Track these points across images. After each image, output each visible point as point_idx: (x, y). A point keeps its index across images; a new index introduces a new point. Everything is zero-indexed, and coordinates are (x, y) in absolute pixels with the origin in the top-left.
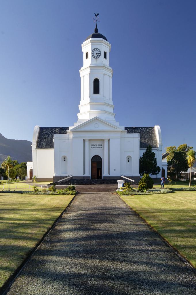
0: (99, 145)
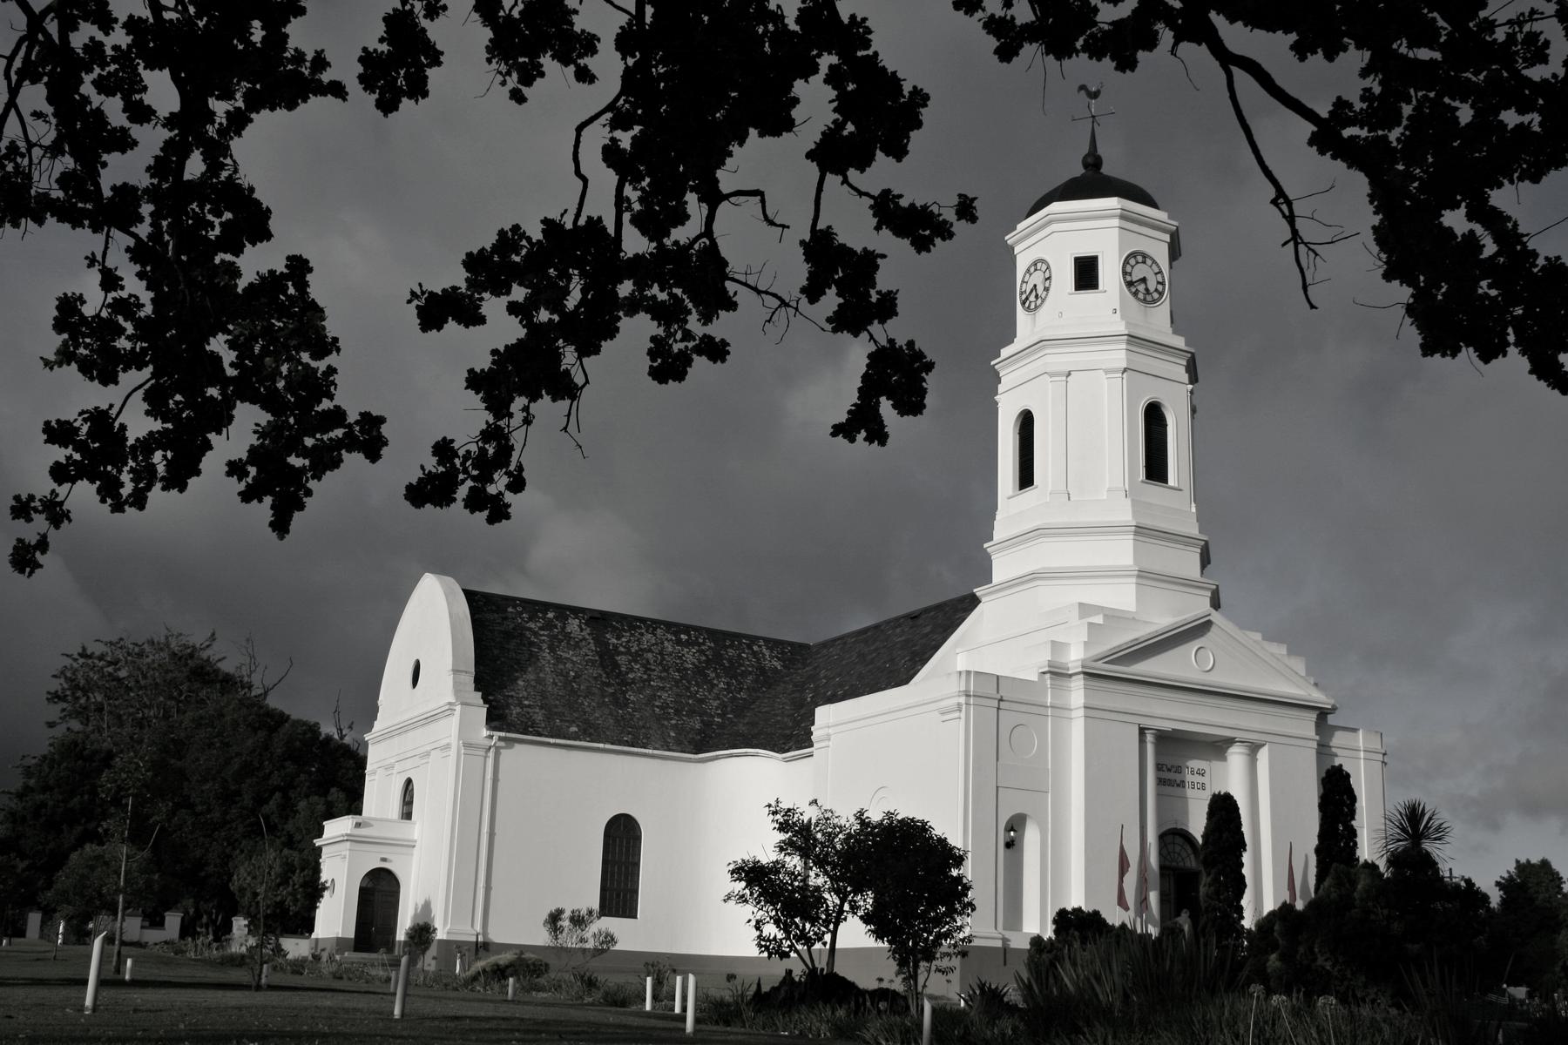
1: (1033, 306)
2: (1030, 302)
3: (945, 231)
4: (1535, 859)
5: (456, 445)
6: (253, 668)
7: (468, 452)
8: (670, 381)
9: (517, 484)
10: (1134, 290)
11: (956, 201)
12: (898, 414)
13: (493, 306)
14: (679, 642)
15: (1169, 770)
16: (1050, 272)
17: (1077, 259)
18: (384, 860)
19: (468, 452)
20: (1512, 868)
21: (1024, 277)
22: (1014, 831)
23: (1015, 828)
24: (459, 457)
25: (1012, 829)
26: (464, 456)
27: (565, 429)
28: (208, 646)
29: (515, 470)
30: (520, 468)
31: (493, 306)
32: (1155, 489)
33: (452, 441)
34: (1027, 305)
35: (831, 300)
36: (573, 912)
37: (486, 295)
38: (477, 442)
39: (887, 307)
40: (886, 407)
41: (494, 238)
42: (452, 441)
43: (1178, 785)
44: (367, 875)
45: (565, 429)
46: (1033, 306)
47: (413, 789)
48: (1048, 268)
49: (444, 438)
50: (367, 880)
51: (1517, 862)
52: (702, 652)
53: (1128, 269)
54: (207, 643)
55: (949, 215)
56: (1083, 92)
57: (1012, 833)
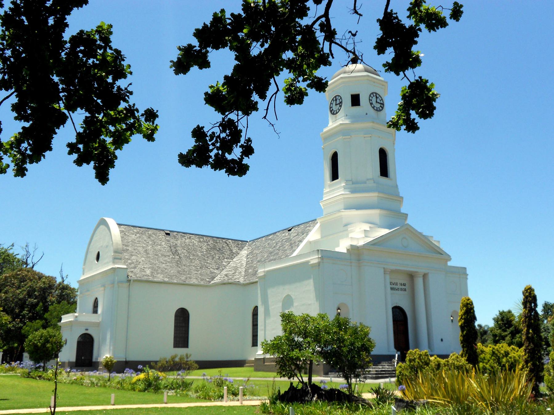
0: (401, 285)
1: (335, 112)
2: (334, 111)
3: (442, 23)
4: (506, 310)
5: (205, 130)
6: (28, 256)
7: (213, 133)
8: (296, 104)
9: (248, 150)
10: (381, 101)
11: (451, 7)
12: (419, 117)
13: (213, 55)
14: (200, 241)
15: (393, 284)
16: (342, 100)
17: (351, 95)
18: (87, 330)
19: (213, 133)
20: (498, 314)
21: (331, 101)
22: (340, 310)
23: (340, 308)
24: (208, 137)
25: (339, 309)
26: (210, 135)
27: (265, 117)
28: (11, 249)
29: (245, 143)
30: (249, 140)
31: (213, 55)
32: (384, 179)
33: (203, 127)
34: (333, 112)
35: (390, 54)
36: (181, 356)
37: (209, 49)
38: (219, 127)
39: (416, 62)
40: (413, 115)
41: (211, 18)
42: (203, 127)
43: (397, 290)
44: (80, 336)
45: (265, 117)
46: (335, 112)
47: (98, 302)
48: (341, 98)
49: (198, 126)
50: (80, 338)
51: (499, 311)
52: (208, 245)
53: (371, 98)
54: (11, 247)
55: (446, 14)
56: (350, 33)
57: (339, 311)
